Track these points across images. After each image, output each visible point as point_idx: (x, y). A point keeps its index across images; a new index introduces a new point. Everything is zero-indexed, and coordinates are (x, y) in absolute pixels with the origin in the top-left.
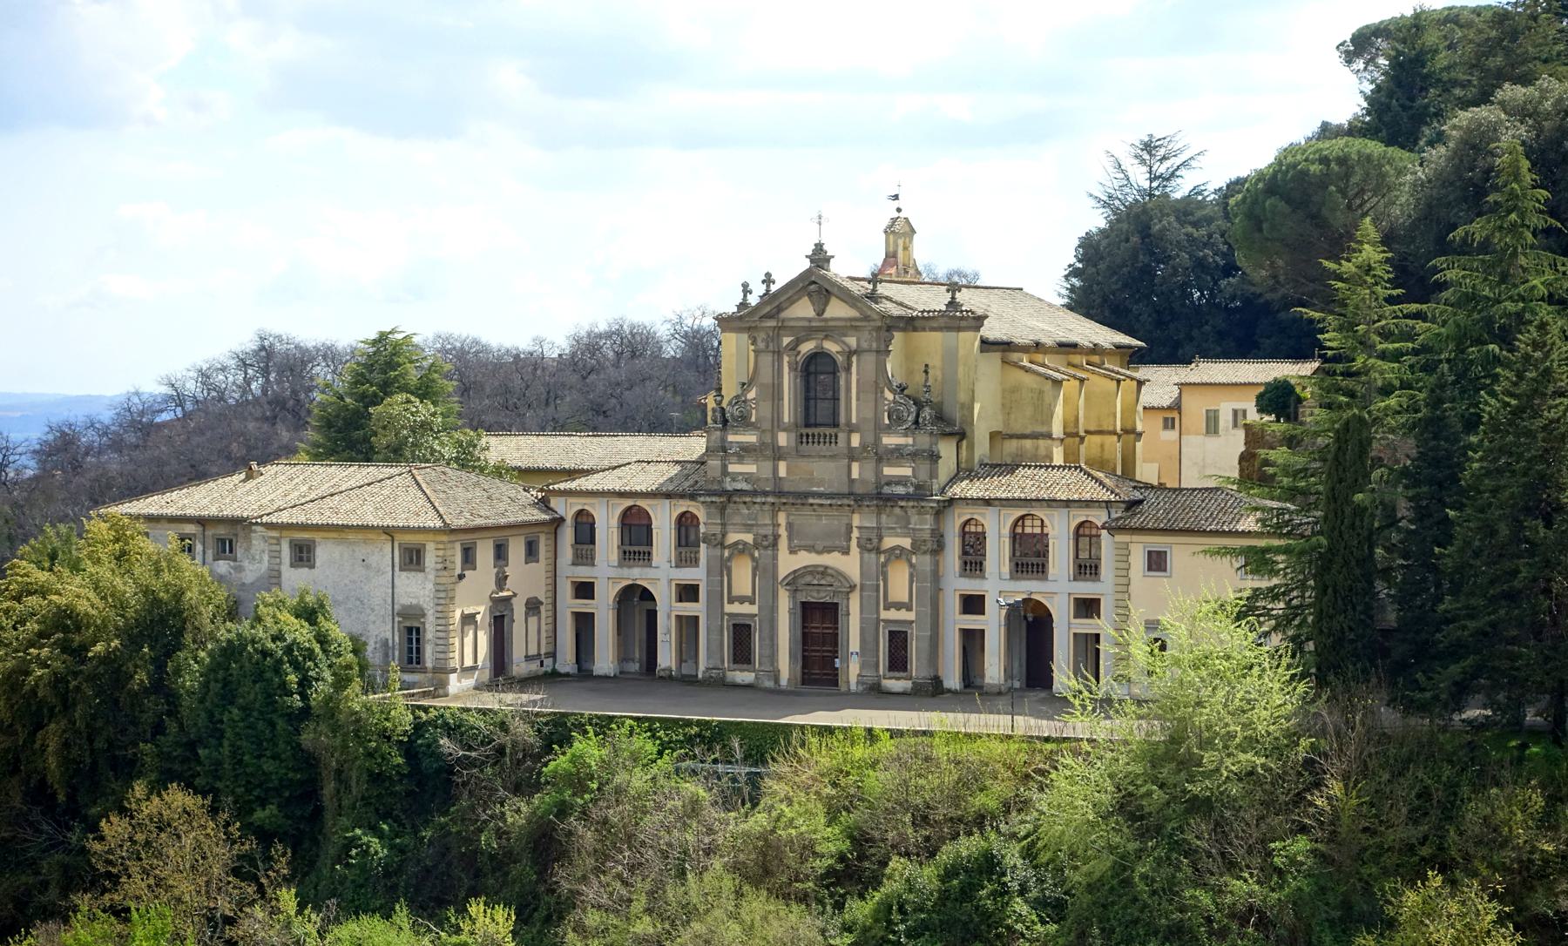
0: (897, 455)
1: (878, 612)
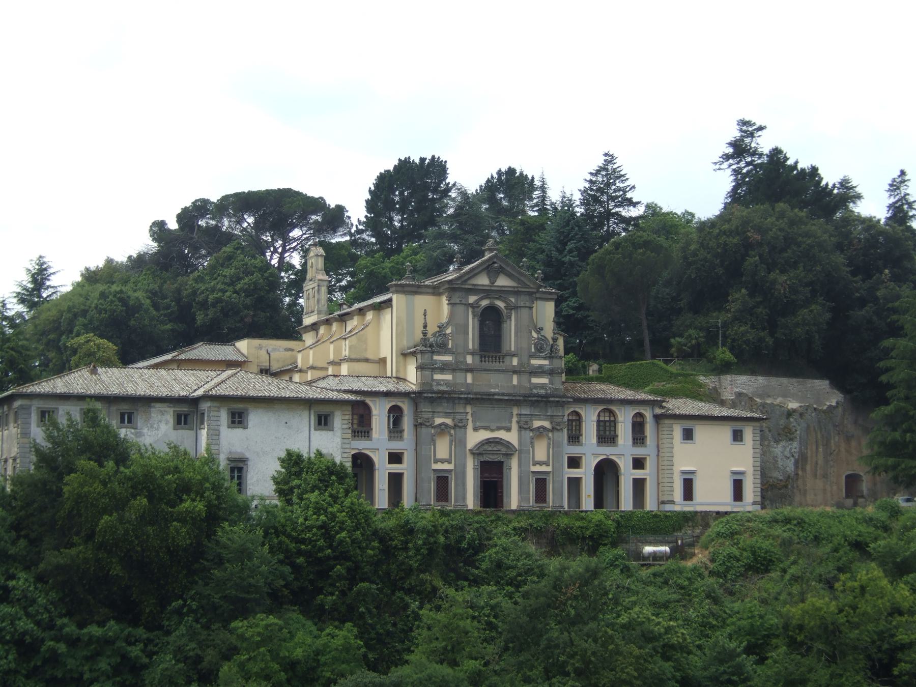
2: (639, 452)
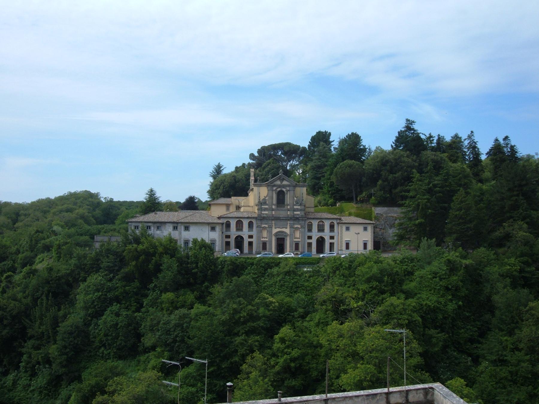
2: (332, 234)
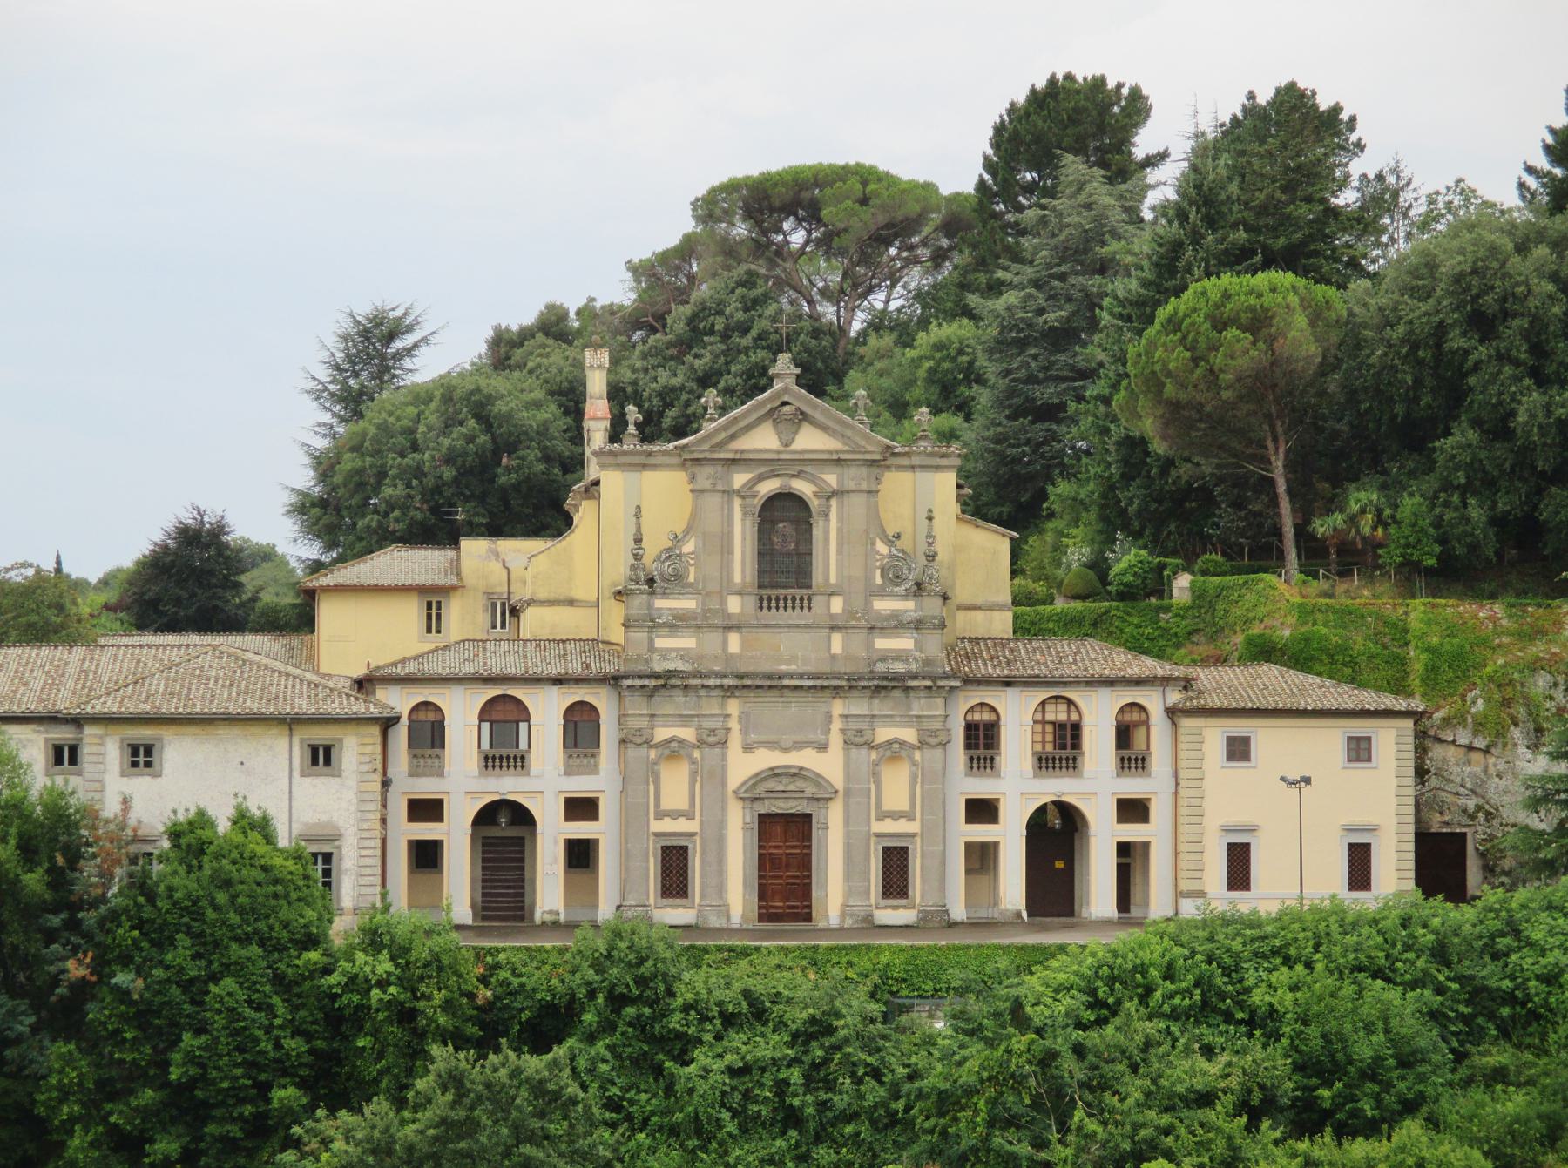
0: (895, 624)
1: (869, 824)
2: (1133, 787)
